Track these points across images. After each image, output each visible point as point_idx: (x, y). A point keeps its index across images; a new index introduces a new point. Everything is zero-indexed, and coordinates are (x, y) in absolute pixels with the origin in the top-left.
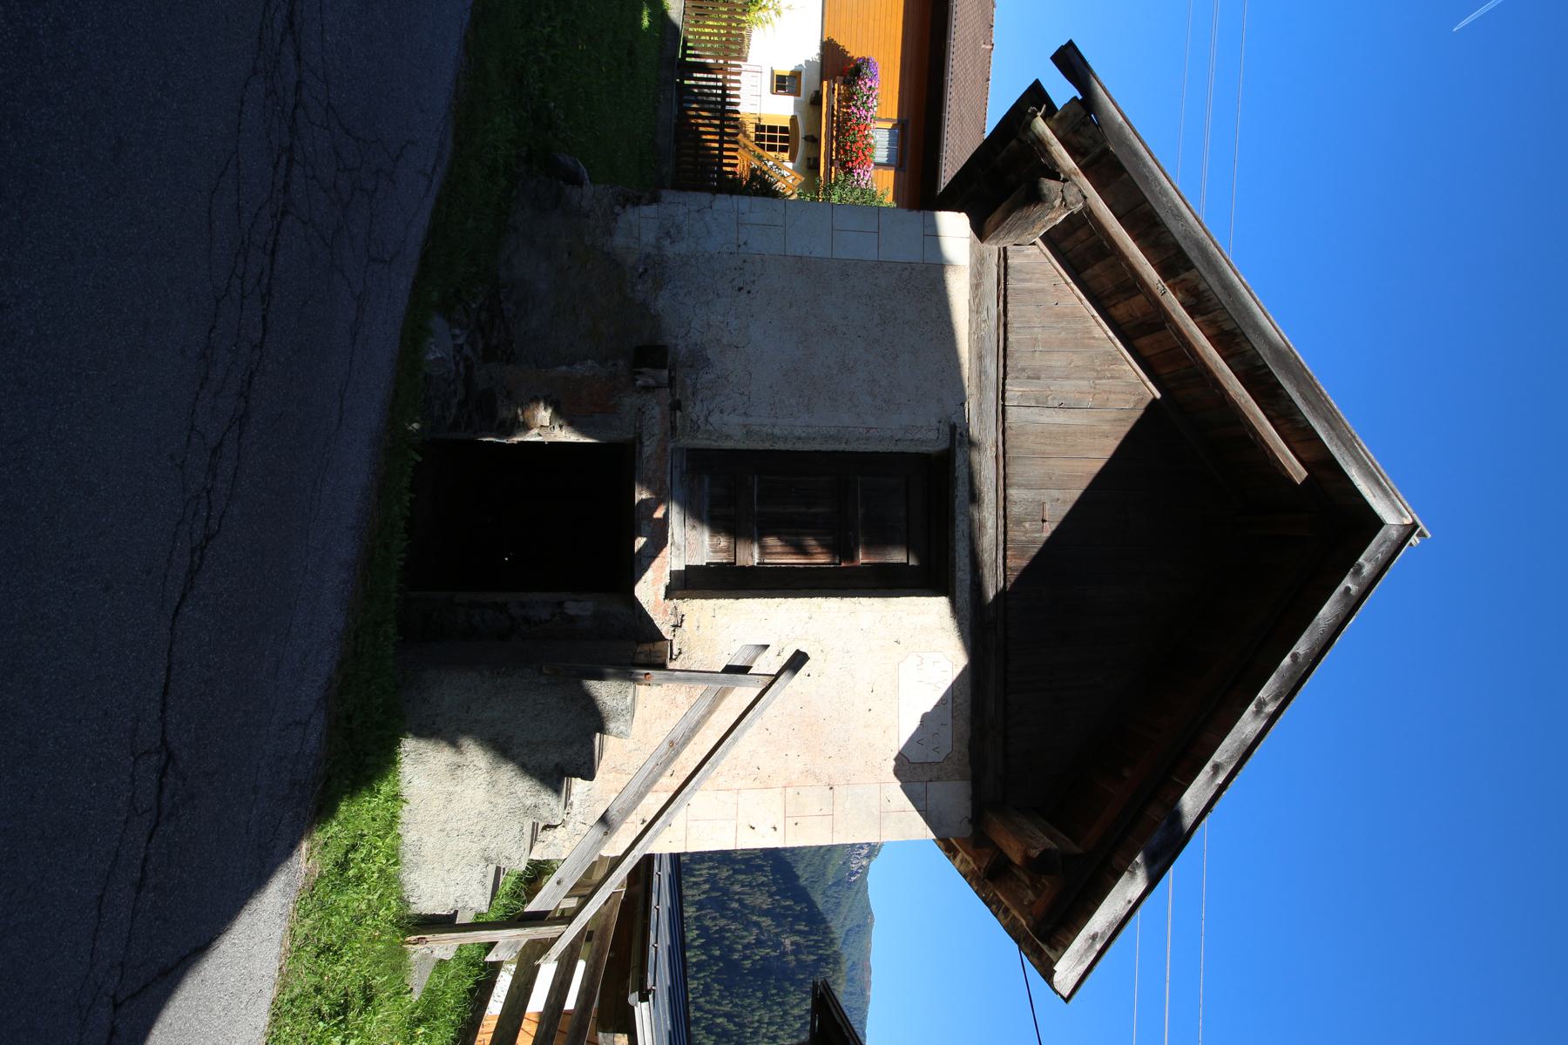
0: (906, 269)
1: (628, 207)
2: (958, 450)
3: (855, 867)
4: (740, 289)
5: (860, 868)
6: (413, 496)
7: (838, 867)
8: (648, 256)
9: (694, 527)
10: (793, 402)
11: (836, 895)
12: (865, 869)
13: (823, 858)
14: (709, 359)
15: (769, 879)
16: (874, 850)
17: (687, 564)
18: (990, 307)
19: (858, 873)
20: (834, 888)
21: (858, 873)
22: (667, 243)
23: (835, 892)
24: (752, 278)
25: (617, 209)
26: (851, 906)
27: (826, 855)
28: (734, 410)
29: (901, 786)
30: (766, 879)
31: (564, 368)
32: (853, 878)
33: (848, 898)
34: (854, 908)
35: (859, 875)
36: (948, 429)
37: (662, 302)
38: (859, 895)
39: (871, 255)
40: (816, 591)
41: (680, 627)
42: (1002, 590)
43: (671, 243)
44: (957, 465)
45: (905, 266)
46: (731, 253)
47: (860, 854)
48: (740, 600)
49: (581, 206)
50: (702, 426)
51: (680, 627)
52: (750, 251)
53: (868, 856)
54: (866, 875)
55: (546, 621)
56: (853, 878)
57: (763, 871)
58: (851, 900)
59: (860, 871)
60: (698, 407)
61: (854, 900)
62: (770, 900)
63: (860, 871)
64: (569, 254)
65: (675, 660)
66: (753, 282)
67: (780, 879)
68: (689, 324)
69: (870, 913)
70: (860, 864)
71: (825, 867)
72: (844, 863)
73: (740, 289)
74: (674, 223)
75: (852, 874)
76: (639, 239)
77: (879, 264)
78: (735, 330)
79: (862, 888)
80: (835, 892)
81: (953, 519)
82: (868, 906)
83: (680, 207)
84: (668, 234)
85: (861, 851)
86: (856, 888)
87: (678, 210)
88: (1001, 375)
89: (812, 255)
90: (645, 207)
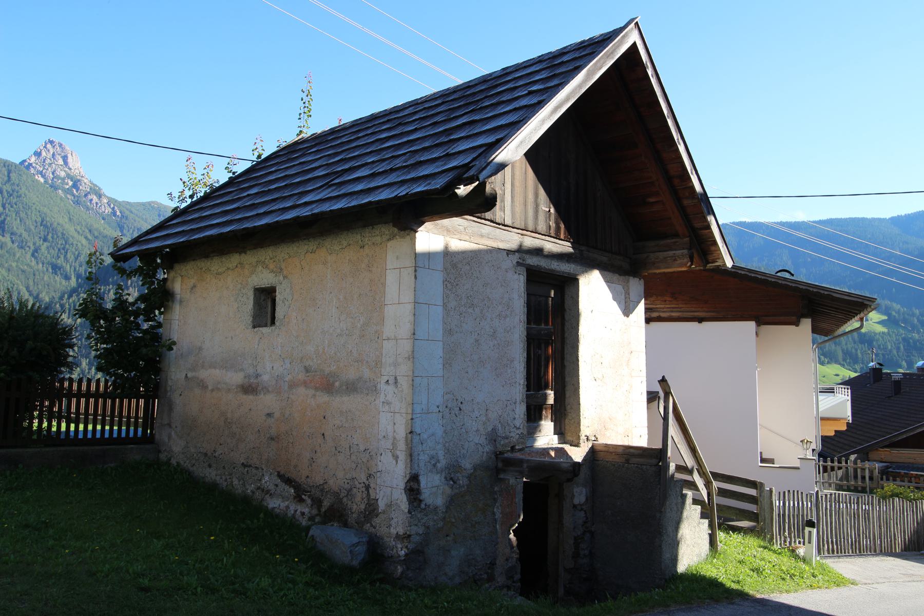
0: (446, 285)
1: (421, 498)
2: (527, 263)
3: (108, 210)
4: (460, 409)
5: (109, 205)
6: (638, 592)
7: (106, 226)
8: (446, 478)
9: (540, 431)
10: (509, 371)
11: (131, 231)
12: (111, 201)
13: (96, 237)
14: (492, 429)
15: (112, 288)
16: (94, 190)
17: (553, 434)
18: (458, 223)
19: (114, 208)
20: (125, 231)
21: (114, 208)
22: (439, 465)
23: (128, 231)
24: (455, 401)
25: (423, 506)
26: (143, 219)
27: (94, 235)
28: (514, 410)
29: (632, 313)
30: (112, 291)
31: (498, 526)
32: (118, 213)
33: (135, 221)
34: (144, 217)
35: (116, 208)
36: (519, 267)
37: (467, 464)
38: (133, 210)
39: (440, 310)
40: (567, 357)
41: (588, 437)
42: (572, 245)
43: (439, 463)
44: (532, 264)
45: (445, 285)
46: (443, 417)
47: (97, 203)
48: (581, 402)
49: (423, 533)
50: (522, 431)
51: (588, 437)
52: (442, 403)
53: (100, 196)
54: (116, 201)
55: (586, 513)
56: (118, 213)
57: (104, 293)
58: (137, 219)
59: (112, 206)
60: (512, 434)
61: (137, 215)
62: (131, 289)
63: (112, 206)
64: (447, 536)
65: (597, 438)
66: (457, 400)
67: (113, 278)
68: (477, 444)
69: (149, 203)
70: (106, 205)
71: (106, 237)
72: (104, 219)
73: (460, 409)
74: (429, 462)
75: (114, 213)
76: (437, 487)
77: (445, 305)
78: (479, 412)
79: (128, 207)
80: (128, 231)
81: (552, 270)
82: (143, 204)
83: (420, 458)
84: (434, 465)
85: (94, 201)
86: (127, 213)
87: (422, 459)
88: (492, 224)
89: (442, 356)
90: (422, 485)
